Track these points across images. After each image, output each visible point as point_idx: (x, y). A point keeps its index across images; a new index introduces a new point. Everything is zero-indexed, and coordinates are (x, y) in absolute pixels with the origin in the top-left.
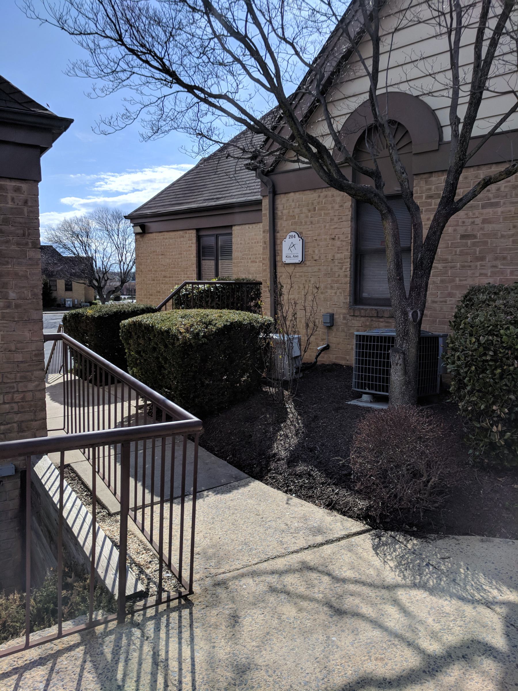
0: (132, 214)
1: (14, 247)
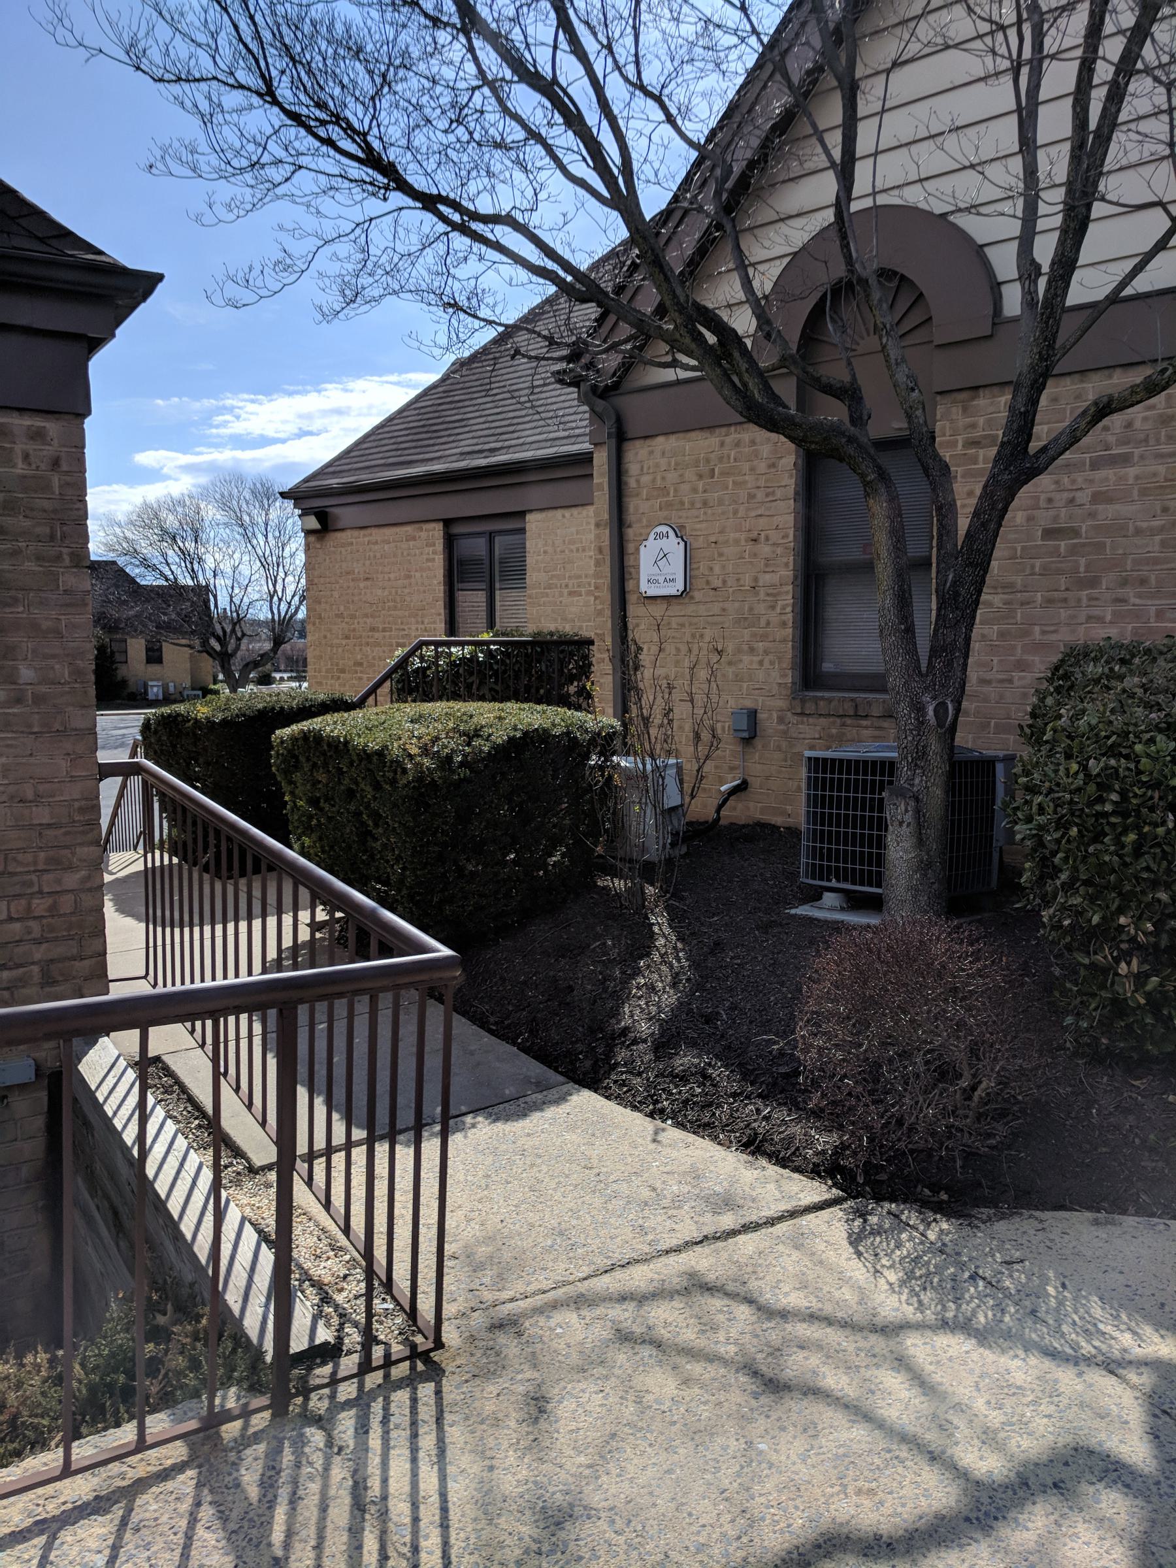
0: (297, 487)
1: (30, 566)
